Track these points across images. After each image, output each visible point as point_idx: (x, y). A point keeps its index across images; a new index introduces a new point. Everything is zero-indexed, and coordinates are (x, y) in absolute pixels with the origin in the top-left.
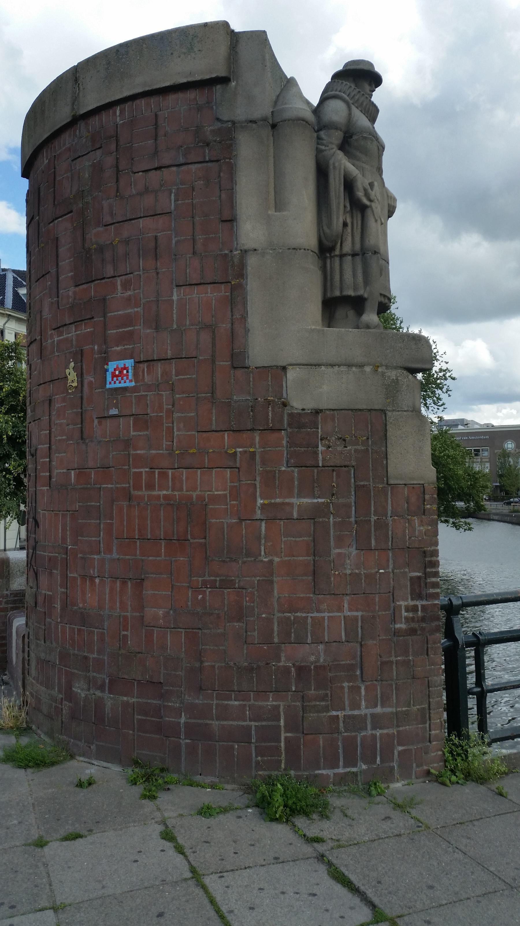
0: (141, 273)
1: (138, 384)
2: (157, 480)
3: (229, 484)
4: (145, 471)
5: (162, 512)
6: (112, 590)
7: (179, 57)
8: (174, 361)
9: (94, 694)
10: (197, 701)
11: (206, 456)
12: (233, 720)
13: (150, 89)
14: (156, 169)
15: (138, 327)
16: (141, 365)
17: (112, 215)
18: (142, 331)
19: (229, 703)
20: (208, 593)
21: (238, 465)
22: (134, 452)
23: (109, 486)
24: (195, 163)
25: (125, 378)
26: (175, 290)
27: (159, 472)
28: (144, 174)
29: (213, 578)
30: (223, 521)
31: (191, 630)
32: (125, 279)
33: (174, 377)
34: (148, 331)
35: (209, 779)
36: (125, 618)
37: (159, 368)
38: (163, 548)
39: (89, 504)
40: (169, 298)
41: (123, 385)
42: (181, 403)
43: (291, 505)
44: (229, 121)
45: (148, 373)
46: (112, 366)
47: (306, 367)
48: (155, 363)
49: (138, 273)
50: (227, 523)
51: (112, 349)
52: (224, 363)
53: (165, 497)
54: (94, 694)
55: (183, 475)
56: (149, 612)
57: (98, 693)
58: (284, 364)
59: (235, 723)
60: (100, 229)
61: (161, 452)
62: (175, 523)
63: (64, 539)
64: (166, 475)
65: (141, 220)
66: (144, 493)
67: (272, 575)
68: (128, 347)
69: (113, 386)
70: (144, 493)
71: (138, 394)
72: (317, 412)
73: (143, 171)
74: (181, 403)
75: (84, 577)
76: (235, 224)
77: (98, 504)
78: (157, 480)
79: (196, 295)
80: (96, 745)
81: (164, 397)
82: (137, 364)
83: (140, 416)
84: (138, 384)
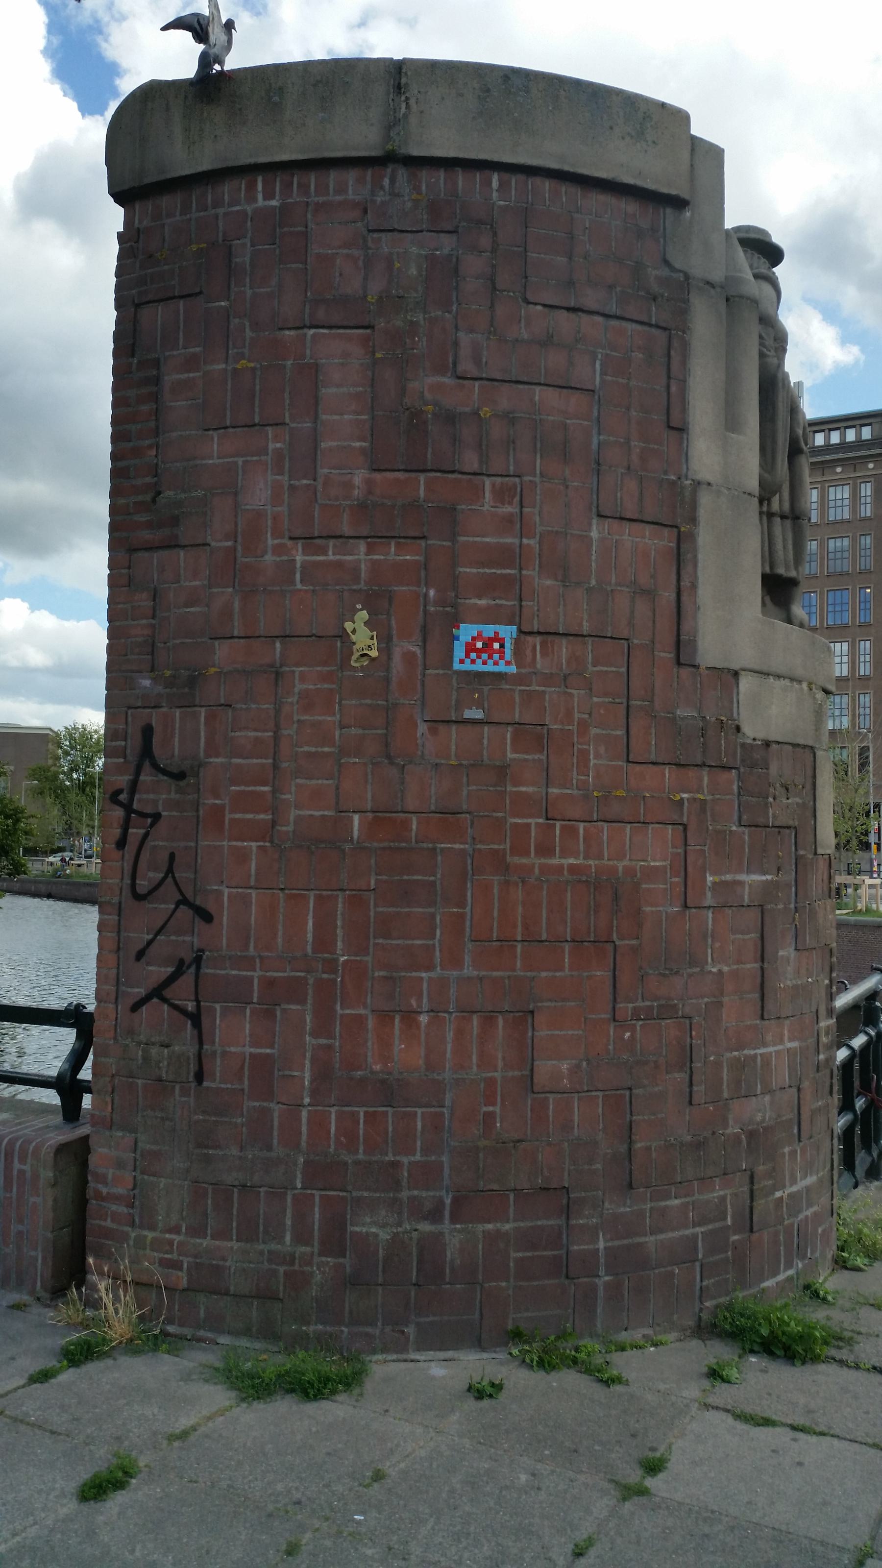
0: (537, 479)
1: (523, 671)
2: (557, 839)
3: (670, 850)
4: (537, 823)
5: (569, 894)
6: (460, 1033)
7: (623, 138)
8: (590, 640)
9: (416, 1230)
10: (622, 1210)
11: (642, 802)
12: (673, 1229)
13: (572, 170)
14: (568, 309)
15: (529, 573)
16: (530, 639)
17: (477, 360)
18: (537, 579)
19: (668, 1203)
20: (638, 1028)
21: (685, 820)
22: (514, 789)
23: (457, 846)
24: (637, 322)
25: (496, 656)
26: (594, 521)
27: (562, 827)
28: (546, 310)
29: (648, 1003)
30: (661, 909)
31: (614, 1092)
32: (502, 483)
33: (590, 666)
34: (549, 582)
35: (637, 1335)
36: (491, 1083)
37: (564, 649)
38: (567, 956)
39: (405, 877)
40: (584, 533)
41: (490, 668)
42: (602, 712)
43: (741, 883)
44: (680, 271)
45: (544, 654)
46: (466, 632)
47: (756, 675)
48: (557, 639)
49: (531, 478)
50: (666, 913)
51: (467, 601)
52: (666, 655)
53: (573, 869)
54: (416, 1230)
55: (602, 832)
56: (544, 1068)
57: (426, 1227)
58: (735, 666)
59: (676, 1234)
60: (447, 380)
61: (569, 791)
62: (592, 913)
63: (324, 942)
64: (574, 831)
65: (538, 389)
66: (534, 860)
67: (722, 994)
68: (504, 602)
69: (467, 666)
70: (534, 860)
71: (528, 688)
72: (767, 744)
73: (545, 306)
74: (602, 712)
75: (385, 1017)
76: (685, 436)
77: (432, 878)
78: (557, 839)
79: (629, 538)
80: (418, 1324)
81: (576, 700)
82: (522, 636)
83: (528, 726)
84: (523, 671)
